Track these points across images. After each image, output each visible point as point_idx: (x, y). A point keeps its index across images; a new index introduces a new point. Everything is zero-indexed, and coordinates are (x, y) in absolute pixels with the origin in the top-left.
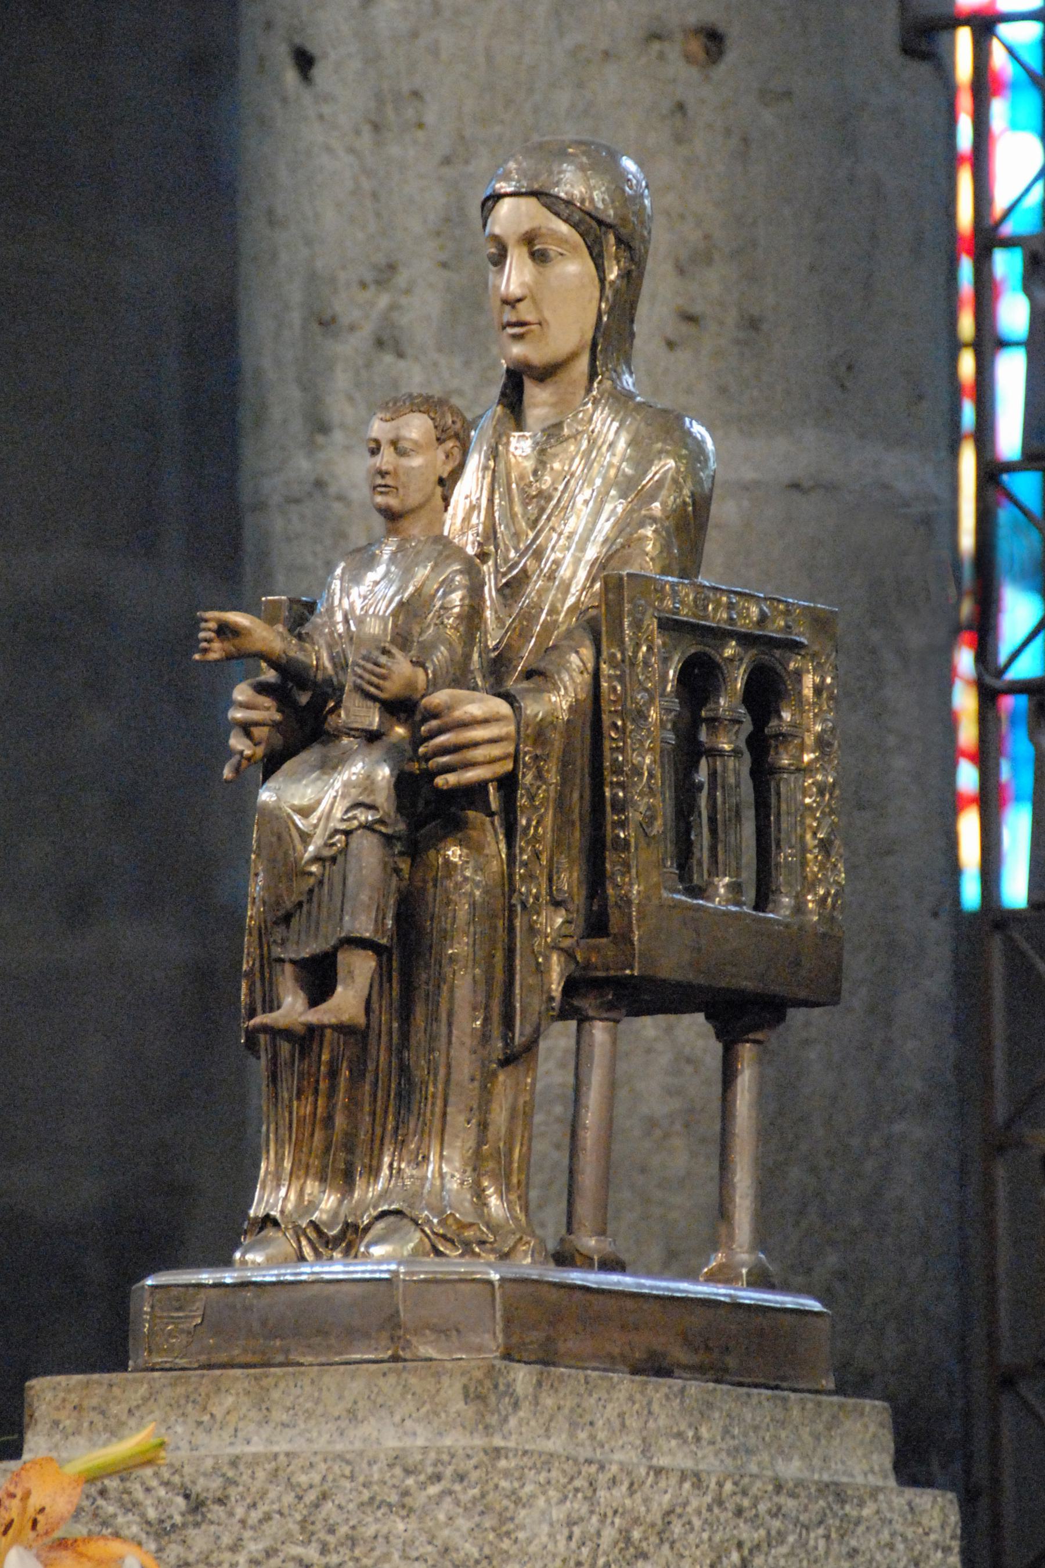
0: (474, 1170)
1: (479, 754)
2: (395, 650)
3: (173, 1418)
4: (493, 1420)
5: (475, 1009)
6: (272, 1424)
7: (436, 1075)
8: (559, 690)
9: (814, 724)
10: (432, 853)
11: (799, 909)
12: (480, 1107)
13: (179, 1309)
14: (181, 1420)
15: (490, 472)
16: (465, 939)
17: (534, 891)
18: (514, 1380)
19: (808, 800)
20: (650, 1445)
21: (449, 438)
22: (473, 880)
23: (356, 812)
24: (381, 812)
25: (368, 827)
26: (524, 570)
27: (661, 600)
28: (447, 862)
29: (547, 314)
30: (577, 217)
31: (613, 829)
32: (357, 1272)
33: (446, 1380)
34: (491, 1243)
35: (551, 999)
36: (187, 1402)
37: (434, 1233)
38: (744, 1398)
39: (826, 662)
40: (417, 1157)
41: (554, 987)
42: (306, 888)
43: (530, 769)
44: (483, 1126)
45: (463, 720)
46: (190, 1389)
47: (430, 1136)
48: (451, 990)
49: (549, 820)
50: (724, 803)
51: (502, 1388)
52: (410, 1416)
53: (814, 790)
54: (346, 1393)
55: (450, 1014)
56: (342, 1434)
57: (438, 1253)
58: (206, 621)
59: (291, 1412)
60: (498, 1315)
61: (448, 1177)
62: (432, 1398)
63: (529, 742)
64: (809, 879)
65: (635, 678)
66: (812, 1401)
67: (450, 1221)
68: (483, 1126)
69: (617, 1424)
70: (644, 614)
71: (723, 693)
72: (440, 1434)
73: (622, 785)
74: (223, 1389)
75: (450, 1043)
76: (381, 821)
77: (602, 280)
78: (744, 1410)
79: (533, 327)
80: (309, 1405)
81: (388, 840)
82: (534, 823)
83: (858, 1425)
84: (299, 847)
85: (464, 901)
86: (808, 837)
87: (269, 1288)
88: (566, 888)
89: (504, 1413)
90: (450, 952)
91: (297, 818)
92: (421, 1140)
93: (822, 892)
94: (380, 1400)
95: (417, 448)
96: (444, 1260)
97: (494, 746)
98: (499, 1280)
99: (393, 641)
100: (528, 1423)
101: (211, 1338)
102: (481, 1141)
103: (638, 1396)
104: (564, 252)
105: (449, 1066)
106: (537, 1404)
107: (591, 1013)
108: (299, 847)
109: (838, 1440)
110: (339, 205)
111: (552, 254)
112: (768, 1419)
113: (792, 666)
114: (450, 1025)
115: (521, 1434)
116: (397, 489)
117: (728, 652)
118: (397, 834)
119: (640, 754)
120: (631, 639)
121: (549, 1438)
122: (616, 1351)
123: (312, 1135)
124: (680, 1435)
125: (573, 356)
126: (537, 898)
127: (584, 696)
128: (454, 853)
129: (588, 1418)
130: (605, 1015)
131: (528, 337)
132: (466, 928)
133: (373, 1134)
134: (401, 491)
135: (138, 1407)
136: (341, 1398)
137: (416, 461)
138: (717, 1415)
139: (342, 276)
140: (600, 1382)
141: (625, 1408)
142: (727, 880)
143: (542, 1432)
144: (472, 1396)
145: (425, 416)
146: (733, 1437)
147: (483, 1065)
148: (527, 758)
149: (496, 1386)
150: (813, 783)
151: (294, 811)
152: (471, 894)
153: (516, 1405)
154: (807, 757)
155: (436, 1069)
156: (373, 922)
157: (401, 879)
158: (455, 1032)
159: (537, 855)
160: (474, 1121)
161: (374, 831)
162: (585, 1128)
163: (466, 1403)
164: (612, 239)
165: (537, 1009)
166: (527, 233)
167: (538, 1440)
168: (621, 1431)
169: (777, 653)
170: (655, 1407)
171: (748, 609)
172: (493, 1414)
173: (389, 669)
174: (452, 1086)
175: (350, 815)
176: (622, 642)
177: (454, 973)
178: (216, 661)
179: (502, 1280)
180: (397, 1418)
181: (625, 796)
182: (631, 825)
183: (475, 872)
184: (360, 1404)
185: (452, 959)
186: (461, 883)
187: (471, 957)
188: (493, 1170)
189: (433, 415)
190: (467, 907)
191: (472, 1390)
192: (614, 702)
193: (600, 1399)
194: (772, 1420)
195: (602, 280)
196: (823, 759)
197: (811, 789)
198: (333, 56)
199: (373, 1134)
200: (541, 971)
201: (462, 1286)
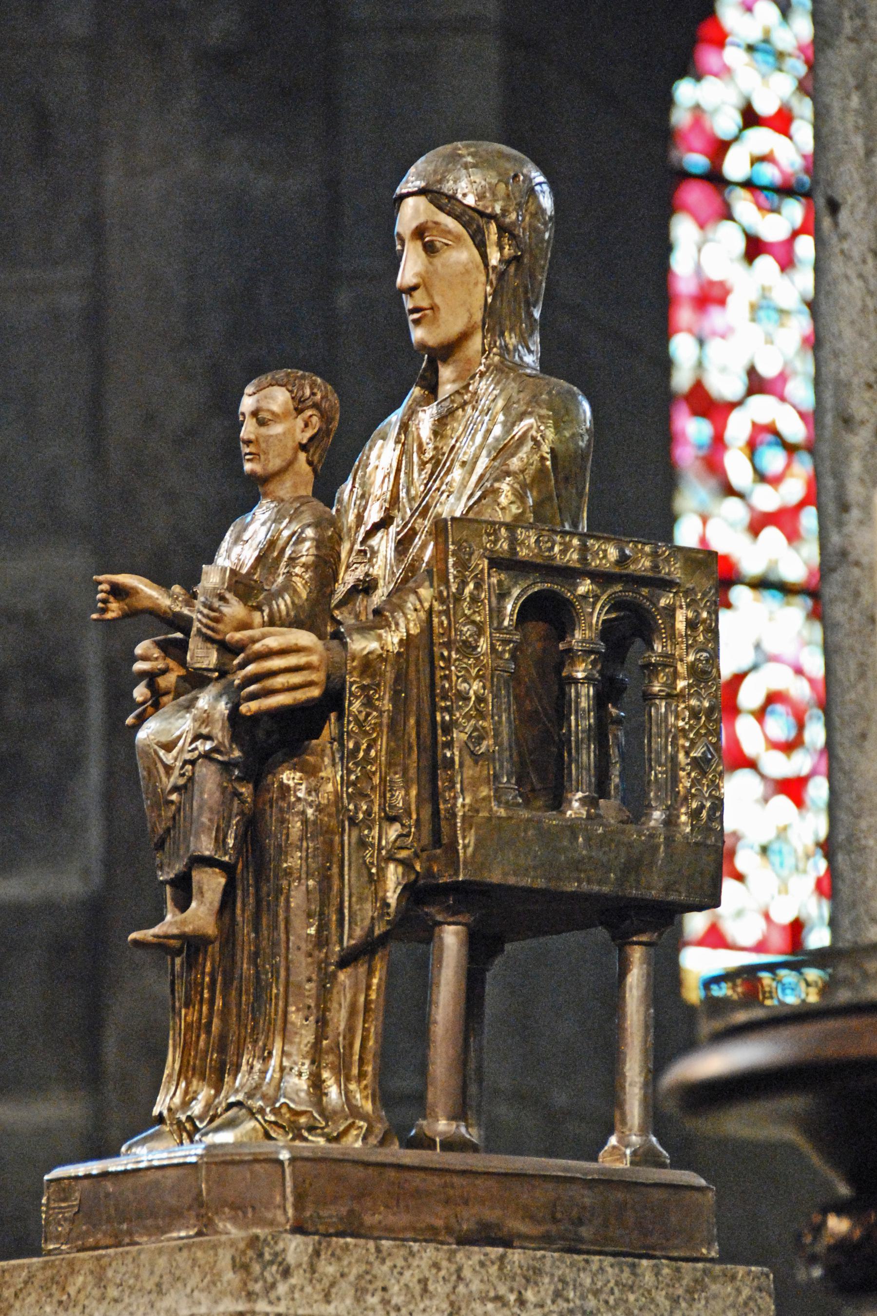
0: (313, 1062)
1: (279, 681)
2: (228, 596)
3: (44, 1299)
4: (258, 1287)
5: (309, 915)
6: (107, 1300)
7: (278, 978)
8: (390, 627)
9: (687, 655)
10: (270, 777)
11: (670, 822)
12: (317, 1006)
13: (64, 1200)
14: (49, 1300)
15: (400, 445)
16: (299, 854)
17: (365, 807)
18: (284, 1250)
19: (681, 723)
20: (460, 1309)
21: (308, 408)
22: (306, 800)
23: (198, 743)
24: (216, 742)
25: (207, 756)
26: (413, 529)
27: (495, 542)
28: (281, 783)
29: (438, 300)
30: (463, 213)
31: (443, 749)
32: (175, 1157)
33: (221, 1251)
34: (322, 1128)
35: (388, 905)
36: (52, 1284)
37: (266, 1121)
38: (582, 1264)
39: (702, 599)
40: (263, 1053)
41: (389, 894)
42: (170, 814)
43: (357, 698)
44: (322, 1023)
45: (260, 652)
46: (55, 1272)
47: (274, 1034)
48: (288, 902)
49: (383, 743)
50: (577, 725)
51: (267, 1257)
52: (197, 1287)
53: (687, 713)
54: (156, 1269)
55: (287, 921)
56: (152, 1306)
57: (268, 1136)
58: (100, 583)
59: (120, 1288)
60: (289, 1190)
61: (287, 1070)
62: (212, 1269)
63: (355, 674)
64: (682, 793)
65: (460, 613)
66: (668, 1266)
67: (284, 1110)
68: (322, 1023)
69: (417, 1289)
70: (471, 554)
71: (577, 627)
72: (216, 1302)
73: (447, 709)
74: (76, 1271)
75: (288, 949)
76: (215, 750)
77: (486, 264)
78: (582, 1275)
79: (427, 312)
80: (131, 1281)
81: (226, 767)
82: (364, 747)
83: (729, 1289)
84: (164, 779)
85: (296, 819)
86: (681, 756)
87: (121, 1176)
88: (401, 805)
89: (270, 1280)
90: (285, 865)
91: (162, 753)
92: (267, 1038)
93: (694, 805)
94: (178, 1273)
95: (276, 417)
96: (272, 1142)
97: (296, 674)
98: (289, 1159)
99: (229, 589)
100: (302, 1289)
101: (84, 1224)
102: (320, 1036)
103: (444, 1264)
104: (450, 243)
105: (288, 969)
106: (314, 1271)
107: (439, 918)
108: (164, 779)
109: (703, 1302)
110: (853, 322)
111: (438, 244)
112: (612, 1284)
113: (663, 602)
114: (287, 932)
115: (293, 1299)
116: (259, 455)
117: (582, 590)
118: (232, 761)
119: (465, 681)
120: (455, 577)
121: (329, 1302)
122: (439, 1223)
123: (198, 1037)
124: (498, 1298)
125: (464, 337)
126: (368, 813)
127: (418, 631)
128: (289, 777)
129: (379, 1284)
130: (451, 919)
131: (423, 321)
132: (299, 843)
133: (239, 1035)
134: (262, 457)
135: (21, 1290)
136: (152, 1273)
137: (277, 429)
138: (547, 1280)
139: (856, 381)
140: (395, 1250)
141: (427, 1274)
142: (580, 795)
143: (320, 1297)
144: (238, 1265)
145: (284, 389)
146: (567, 1300)
147: (320, 969)
148: (353, 688)
149: (261, 1255)
150: (686, 708)
151: (160, 746)
152: (303, 813)
153: (286, 1273)
154: (681, 684)
155: (278, 972)
156: (213, 842)
157: (244, 802)
158: (292, 938)
159: (369, 776)
160: (311, 1018)
161: (212, 760)
162: (436, 1022)
163: (235, 1273)
164: (493, 227)
165: (370, 914)
166: (417, 228)
167: (315, 1306)
168: (422, 1297)
169: (645, 591)
170: (467, 1273)
171: (605, 551)
172: (256, 1281)
173: (221, 612)
174: (291, 989)
175: (193, 746)
176: (448, 580)
177: (289, 885)
178: (114, 620)
179: (293, 1160)
180: (188, 1290)
181: (451, 719)
182: (456, 744)
183: (309, 793)
184: (165, 1278)
185: (288, 873)
186: (294, 803)
187: (304, 869)
188: (332, 1063)
189: (290, 388)
190: (299, 824)
191: (238, 1260)
192: (443, 634)
193: (395, 1266)
194: (617, 1284)
195: (486, 264)
196: (698, 686)
197: (684, 713)
198: (850, 200)
199: (239, 1035)
200: (376, 881)
201: (257, 1167)
